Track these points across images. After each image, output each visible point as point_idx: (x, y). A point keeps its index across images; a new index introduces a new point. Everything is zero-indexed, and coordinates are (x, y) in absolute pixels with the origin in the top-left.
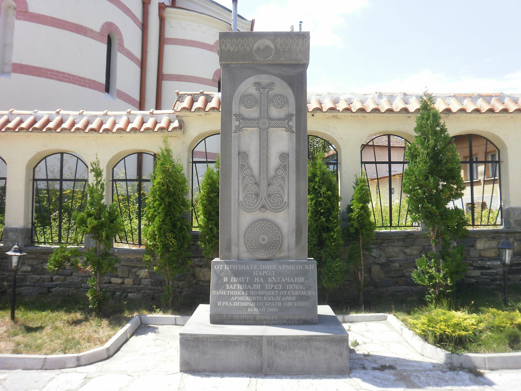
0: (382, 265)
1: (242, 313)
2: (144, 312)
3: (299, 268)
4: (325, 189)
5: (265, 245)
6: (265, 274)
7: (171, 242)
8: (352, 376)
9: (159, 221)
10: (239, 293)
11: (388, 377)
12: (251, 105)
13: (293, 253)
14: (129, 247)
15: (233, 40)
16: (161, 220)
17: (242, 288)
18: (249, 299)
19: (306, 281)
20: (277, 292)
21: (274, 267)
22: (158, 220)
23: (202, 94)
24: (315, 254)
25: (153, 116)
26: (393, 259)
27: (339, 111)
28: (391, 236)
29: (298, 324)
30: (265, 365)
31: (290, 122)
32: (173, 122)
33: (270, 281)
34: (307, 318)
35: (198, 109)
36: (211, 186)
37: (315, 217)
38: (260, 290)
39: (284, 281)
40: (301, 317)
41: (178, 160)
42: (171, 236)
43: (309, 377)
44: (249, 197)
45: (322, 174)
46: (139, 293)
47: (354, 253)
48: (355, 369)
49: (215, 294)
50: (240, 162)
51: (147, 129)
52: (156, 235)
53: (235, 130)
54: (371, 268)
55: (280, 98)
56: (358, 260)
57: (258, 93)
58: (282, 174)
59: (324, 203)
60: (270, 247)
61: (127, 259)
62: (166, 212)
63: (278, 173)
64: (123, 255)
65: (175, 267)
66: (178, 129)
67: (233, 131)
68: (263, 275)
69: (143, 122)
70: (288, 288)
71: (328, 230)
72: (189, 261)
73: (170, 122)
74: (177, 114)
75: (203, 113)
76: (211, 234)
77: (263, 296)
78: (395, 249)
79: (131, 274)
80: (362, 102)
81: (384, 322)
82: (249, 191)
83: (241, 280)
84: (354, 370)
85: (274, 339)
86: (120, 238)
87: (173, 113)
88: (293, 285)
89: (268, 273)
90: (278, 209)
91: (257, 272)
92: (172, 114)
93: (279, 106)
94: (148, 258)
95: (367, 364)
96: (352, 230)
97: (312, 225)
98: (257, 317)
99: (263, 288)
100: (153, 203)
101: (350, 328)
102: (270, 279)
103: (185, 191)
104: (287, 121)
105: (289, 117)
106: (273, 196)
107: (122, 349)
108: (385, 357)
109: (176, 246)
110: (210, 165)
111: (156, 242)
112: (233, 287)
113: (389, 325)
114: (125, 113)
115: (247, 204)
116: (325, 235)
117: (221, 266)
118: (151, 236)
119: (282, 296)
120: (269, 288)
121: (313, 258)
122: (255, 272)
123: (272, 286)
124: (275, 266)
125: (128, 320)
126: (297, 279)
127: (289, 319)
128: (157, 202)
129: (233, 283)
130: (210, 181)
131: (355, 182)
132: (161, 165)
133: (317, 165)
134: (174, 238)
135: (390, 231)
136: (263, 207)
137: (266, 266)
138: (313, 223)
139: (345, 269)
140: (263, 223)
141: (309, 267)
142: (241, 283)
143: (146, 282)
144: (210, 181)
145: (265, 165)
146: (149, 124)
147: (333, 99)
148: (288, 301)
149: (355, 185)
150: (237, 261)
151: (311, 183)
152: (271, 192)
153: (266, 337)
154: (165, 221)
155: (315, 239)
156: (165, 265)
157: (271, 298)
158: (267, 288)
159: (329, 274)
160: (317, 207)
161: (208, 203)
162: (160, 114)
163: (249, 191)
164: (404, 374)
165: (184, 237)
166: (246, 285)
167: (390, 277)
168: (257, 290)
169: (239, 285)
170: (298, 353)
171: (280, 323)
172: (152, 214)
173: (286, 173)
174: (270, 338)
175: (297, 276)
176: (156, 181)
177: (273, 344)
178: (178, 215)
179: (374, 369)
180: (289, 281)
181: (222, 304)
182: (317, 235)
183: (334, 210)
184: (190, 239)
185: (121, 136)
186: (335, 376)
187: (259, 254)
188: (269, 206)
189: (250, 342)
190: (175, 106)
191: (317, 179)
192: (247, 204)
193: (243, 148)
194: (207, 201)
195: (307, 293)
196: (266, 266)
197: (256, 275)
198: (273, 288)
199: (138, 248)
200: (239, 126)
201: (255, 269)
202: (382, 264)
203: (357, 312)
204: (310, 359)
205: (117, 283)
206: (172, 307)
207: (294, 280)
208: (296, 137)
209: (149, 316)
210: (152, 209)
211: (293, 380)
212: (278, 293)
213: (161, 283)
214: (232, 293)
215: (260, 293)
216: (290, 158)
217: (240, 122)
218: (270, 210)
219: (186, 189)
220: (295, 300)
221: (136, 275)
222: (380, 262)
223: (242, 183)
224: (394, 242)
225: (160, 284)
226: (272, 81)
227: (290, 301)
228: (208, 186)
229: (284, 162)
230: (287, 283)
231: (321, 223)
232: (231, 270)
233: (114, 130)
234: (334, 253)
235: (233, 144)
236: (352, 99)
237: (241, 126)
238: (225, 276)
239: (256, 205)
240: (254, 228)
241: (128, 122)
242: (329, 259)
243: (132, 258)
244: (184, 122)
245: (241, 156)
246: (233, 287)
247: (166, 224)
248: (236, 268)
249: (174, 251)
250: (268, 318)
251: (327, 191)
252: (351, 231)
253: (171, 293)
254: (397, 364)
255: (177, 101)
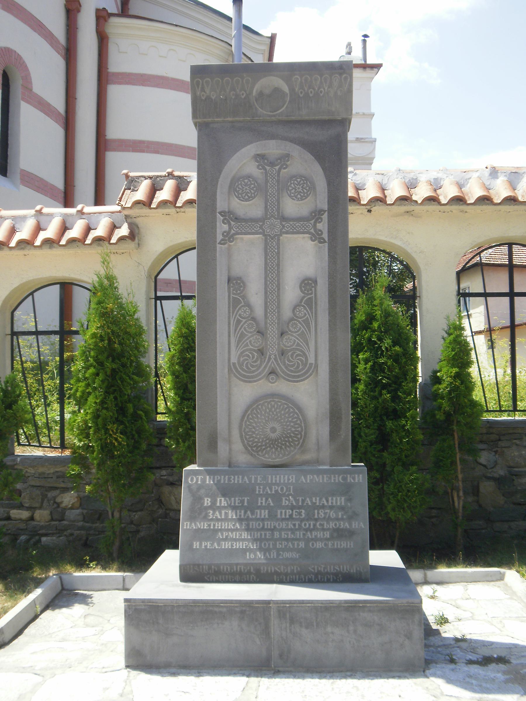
0: (499, 481)
1: (236, 562)
2: (68, 567)
3: (337, 481)
4: (389, 341)
5: (276, 440)
6: (276, 491)
7: (116, 439)
8: (428, 675)
9: (96, 403)
10: (231, 526)
11: (492, 675)
12: (249, 195)
13: (326, 453)
14: (42, 453)
15: (226, 79)
16: (98, 401)
17: (236, 516)
18: (247, 536)
19: (349, 504)
20: (297, 523)
21: (293, 479)
22: (94, 401)
23: (170, 175)
24: (373, 459)
25: (84, 217)
26: (520, 469)
27: (416, 202)
28: (514, 428)
29: (335, 581)
30: (275, 653)
31: (318, 224)
32: (120, 227)
33: (285, 503)
34: (350, 569)
35: (164, 203)
36: (187, 339)
37: (372, 391)
38: (268, 520)
39: (310, 504)
40: (340, 568)
41: (128, 295)
42: (117, 429)
43: (351, 676)
44: (248, 356)
45: (385, 316)
46: (59, 536)
47: (443, 457)
48: (436, 663)
49: (188, 527)
50: (232, 295)
51: (72, 241)
52: (90, 428)
53: (222, 240)
54: (478, 487)
55: (300, 181)
56: (451, 470)
57: (262, 173)
58: (305, 314)
59: (389, 368)
60: (285, 444)
61: (40, 474)
62: (108, 387)
63: (298, 313)
64: (31, 467)
65: (124, 485)
66: (127, 239)
67: (218, 241)
68: (273, 492)
69: (64, 228)
70: (316, 517)
71: (396, 415)
72: (149, 474)
73: (114, 227)
74: (126, 212)
75: (172, 211)
76: (187, 424)
77: (273, 530)
78: (524, 452)
79: (46, 501)
80: (460, 186)
81: (498, 583)
82: (248, 346)
83: (235, 503)
84: (434, 664)
85: (290, 606)
86: (27, 437)
87: (120, 212)
88: (326, 511)
89: (282, 489)
90: (298, 376)
91: (262, 487)
92: (117, 212)
93: (299, 196)
94: (75, 470)
95: (458, 654)
96: (440, 416)
97: (366, 407)
98: (262, 568)
99: (272, 516)
100: (85, 372)
101: (434, 592)
102: (286, 499)
103: (142, 349)
104: (312, 222)
105: (317, 214)
106: (290, 354)
107: (26, 631)
108: (492, 643)
109: (126, 447)
110: (186, 302)
111: (90, 440)
112: (221, 516)
113: (507, 589)
114: (33, 212)
115: (245, 368)
116: (389, 424)
117: (200, 479)
118: (82, 430)
119: (306, 530)
120: (283, 517)
121: (363, 464)
122: (260, 488)
123: (289, 512)
124: (294, 476)
125: (38, 583)
126: (332, 499)
127: (319, 573)
128: (92, 370)
129: (220, 508)
130: (184, 330)
131: (446, 329)
132: (97, 304)
133: (375, 300)
134: (121, 433)
135: (513, 418)
136: (273, 372)
137: (278, 476)
138: (368, 402)
139: (427, 485)
140: (274, 401)
141: (354, 479)
142: (234, 508)
143: (73, 515)
144: (184, 330)
145: (274, 300)
146: (75, 232)
147: (407, 181)
148: (316, 539)
149: (446, 335)
150: (227, 468)
151: (365, 331)
152: (285, 346)
153: (275, 604)
154: (106, 403)
155: (373, 431)
156: (107, 481)
157: (288, 535)
158: (279, 516)
159: (397, 495)
160: (375, 374)
161: (182, 369)
162: (95, 213)
163: (248, 346)
164: (521, 672)
165: (139, 432)
166: (243, 512)
167: (514, 504)
168: (263, 520)
169: (230, 511)
170: (333, 633)
171: (304, 579)
172: (83, 392)
173: (312, 313)
174: (282, 605)
175: (333, 495)
176: (89, 333)
177: (288, 616)
178: (129, 391)
179: (470, 662)
180: (318, 504)
181: (201, 545)
182: (376, 425)
183: (406, 379)
184: (151, 435)
185: (25, 253)
186: (398, 674)
187: (267, 456)
188: (283, 372)
189: (247, 613)
190: (121, 198)
191: (376, 325)
192: (245, 368)
193: (237, 271)
194: (180, 366)
195: (350, 524)
196: (278, 476)
197: (261, 492)
198: (291, 516)
199: (60, 455)
200: (228, 233)
201: (259, 482)
202: (499, 479)
203: (449, 566)
204: (354, 643)
205: (21, 519)
206: (118, 558)
207: (327, 501)
208: (329, 250)
209: (77, 574)
210: (82, 382)
211: (324, 681)
212: (299, 525)
213: (101, 516)
214: (218, 525)
215: (268, 524)
216: (319, 287)
217: (230, 224)
218: (285, 379)
219: (144, 346)
220: (328, 537)
221: (55, 502)
222: (496, 475)
223: (235, 333)
224: (521, 439)
225: (99, 519)
226: (286, 152)
227: (321, 540)
228: (181, 339)
229: (308, 295)
230: (315, 507)
231: (383, 402)
232: (218, 484)
233: (13, 244)
234: (406, 457)
235: (218, 263)
236: (441, 179)
237: (233, 232)
238: (207, 496)
239: (260, 370)
240: (256, 411)
241: (38, 229)
242: (398, 468)
243: (49, 472)
244: (138, 227)
245: (233, 284)
246: (221, 516)
247: (107, 409)
248: (226, 482)
249: (122, 456)
250: (282, 571)
251: (394, 346)
252: (438, 417)
253: (118, 533)
254: (512, 655)
255: (125, 189)
